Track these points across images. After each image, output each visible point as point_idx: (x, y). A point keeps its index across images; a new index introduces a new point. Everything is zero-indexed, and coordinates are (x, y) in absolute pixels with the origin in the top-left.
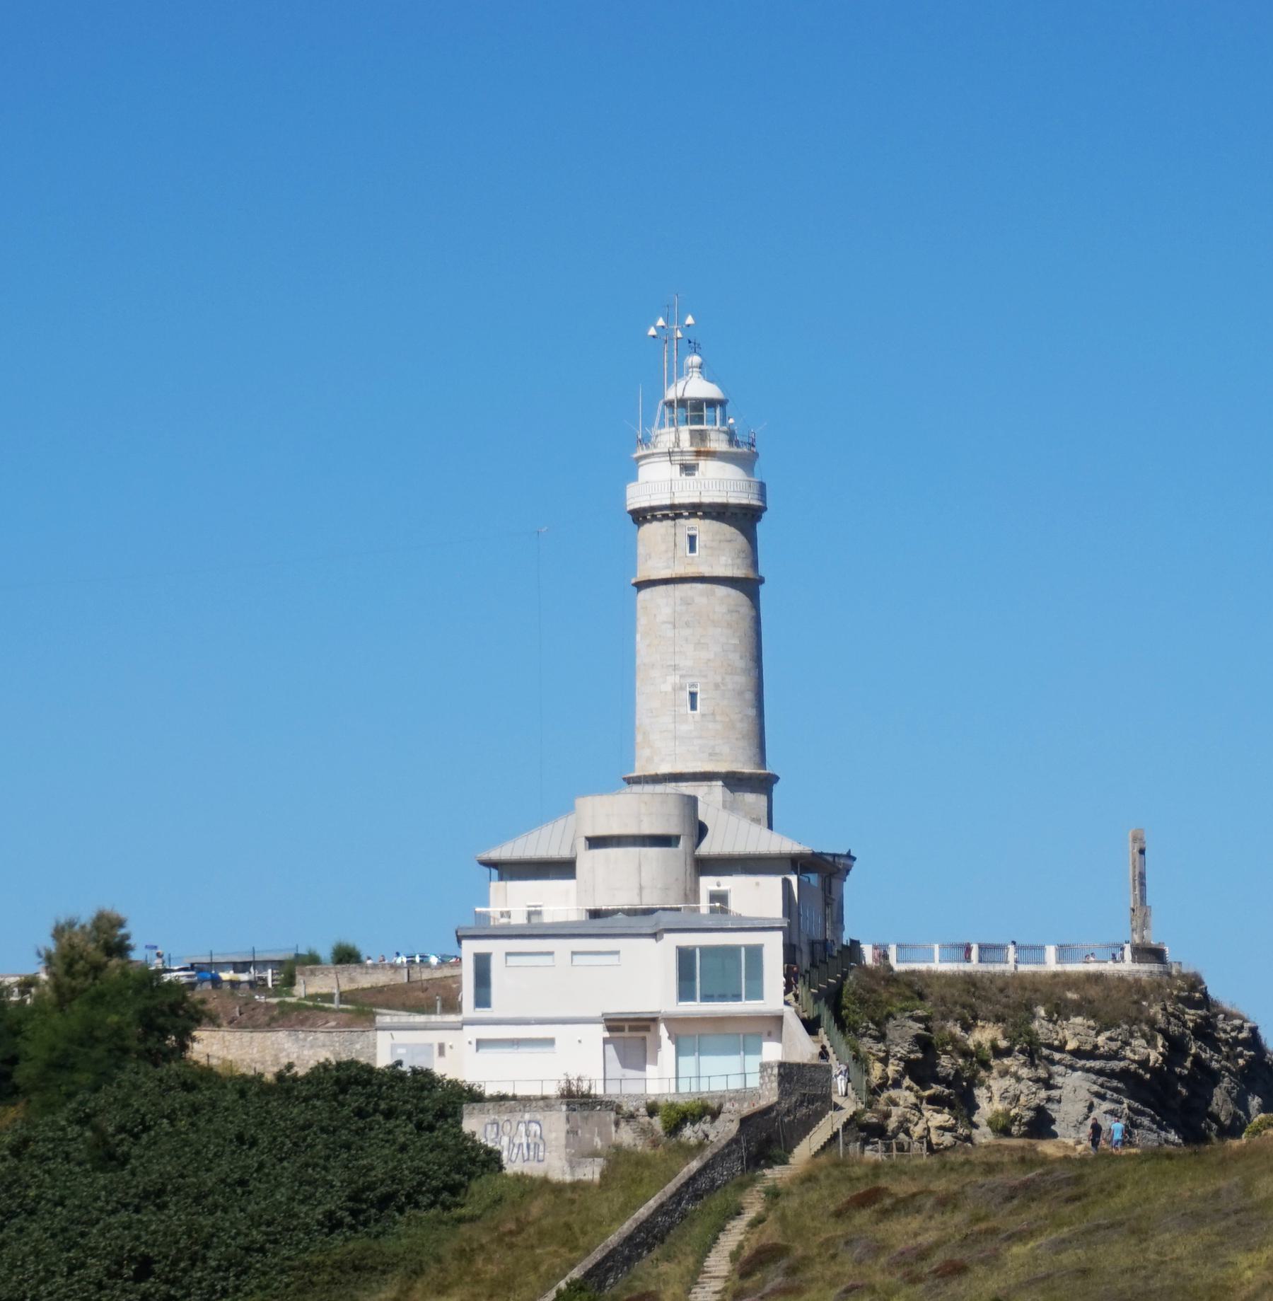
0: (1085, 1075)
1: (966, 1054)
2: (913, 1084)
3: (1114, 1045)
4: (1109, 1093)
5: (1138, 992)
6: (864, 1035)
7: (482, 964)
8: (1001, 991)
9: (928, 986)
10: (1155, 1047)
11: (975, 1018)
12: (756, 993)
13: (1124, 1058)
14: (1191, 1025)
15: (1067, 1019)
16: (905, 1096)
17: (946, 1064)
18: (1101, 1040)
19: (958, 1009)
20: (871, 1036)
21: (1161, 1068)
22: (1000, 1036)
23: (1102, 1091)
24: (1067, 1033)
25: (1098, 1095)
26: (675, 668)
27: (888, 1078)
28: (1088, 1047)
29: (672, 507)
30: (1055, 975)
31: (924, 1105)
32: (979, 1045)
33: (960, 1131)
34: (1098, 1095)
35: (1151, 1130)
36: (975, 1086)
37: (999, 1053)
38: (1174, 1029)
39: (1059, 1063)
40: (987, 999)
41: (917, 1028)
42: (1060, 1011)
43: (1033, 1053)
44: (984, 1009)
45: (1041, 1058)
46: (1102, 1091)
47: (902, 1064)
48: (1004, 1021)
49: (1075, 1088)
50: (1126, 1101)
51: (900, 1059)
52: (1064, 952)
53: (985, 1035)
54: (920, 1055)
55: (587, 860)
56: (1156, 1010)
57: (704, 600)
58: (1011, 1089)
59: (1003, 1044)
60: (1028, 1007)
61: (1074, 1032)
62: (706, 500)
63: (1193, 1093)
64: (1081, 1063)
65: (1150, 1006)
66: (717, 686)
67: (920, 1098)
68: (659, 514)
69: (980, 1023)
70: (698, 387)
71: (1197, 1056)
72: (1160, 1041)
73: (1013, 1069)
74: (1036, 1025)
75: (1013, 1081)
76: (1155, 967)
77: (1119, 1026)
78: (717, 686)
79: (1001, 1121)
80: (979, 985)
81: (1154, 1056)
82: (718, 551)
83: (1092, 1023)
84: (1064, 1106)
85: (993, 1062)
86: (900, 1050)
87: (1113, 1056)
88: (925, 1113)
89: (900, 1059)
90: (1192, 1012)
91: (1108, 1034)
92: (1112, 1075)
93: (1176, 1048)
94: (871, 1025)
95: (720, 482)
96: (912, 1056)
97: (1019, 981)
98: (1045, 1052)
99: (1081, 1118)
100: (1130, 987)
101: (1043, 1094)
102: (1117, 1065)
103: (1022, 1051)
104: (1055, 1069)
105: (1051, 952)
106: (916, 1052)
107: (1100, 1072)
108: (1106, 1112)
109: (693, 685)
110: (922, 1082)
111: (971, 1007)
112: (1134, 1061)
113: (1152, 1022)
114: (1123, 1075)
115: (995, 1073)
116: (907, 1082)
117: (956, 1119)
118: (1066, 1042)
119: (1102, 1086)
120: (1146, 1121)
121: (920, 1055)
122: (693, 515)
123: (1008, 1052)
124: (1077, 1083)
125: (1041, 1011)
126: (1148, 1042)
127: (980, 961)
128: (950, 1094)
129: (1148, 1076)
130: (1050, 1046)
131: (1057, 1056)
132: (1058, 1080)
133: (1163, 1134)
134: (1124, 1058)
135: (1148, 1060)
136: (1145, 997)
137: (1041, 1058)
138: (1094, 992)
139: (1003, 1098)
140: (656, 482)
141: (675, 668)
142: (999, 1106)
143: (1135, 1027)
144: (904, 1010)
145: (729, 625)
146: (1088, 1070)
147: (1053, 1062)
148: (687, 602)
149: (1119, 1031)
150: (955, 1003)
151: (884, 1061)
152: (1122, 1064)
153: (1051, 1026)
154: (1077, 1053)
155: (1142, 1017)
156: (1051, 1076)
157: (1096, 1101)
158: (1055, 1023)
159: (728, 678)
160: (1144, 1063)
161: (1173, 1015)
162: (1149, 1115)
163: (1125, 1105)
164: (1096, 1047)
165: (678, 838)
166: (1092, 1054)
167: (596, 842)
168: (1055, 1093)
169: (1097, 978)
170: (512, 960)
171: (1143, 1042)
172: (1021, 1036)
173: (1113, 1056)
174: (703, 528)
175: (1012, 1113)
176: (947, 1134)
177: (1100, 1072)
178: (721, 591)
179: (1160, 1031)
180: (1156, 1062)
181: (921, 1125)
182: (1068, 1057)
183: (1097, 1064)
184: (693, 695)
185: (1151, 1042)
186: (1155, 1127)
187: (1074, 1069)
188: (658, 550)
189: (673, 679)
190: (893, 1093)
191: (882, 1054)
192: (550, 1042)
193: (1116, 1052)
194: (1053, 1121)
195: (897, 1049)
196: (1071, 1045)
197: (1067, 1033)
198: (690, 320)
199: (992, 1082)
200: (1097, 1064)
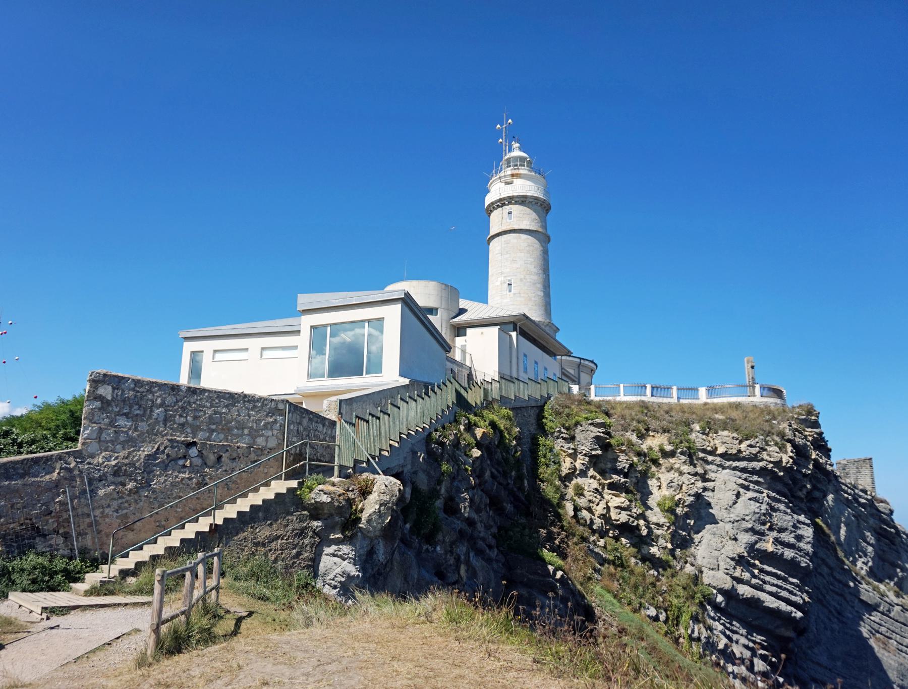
0: (732, 472)
1: (639, 454)
2: (596, 474)
3: (754, 451)
4: (752, 486)
5: (769, 414)
6: (558, 438)
8: (667, 412)
9: (613, 408)
10: (786, 452)
11: (647, 430)
12: (376, 367)
13: (762, 460)
14: (810, 439)
15: (716, 432)
16: (589, 483)
17: (623, 462)
18: (743, 446)
19: (635, 423)
20: (564, 439)
21: (791, 468)
22: (666, 442)
23: (747, 484)
24: (716, 442)
25: (742, 486)
26: (502, 273)
27: (575, 469)
28: (734, 452)
29: (500, 200)
30: (706, 404)
31: (606, 490)
32: (651, 449)
33: (634, 510)
34: (742, 486)
35: (786, 513)
36: (648, 478)
38: (799, 440)
39: (711, 463)
40: (657, 418)
41: (596, 431)
42: (709, 428)
43: (691, 455)
45: (698, 459)
46: (747, 484)
47: (587, 459)
48: (668, 431)
49: (724, 485)
50: (765, 491)
51: (585, 455)
52: (711, 391)
53: (655, 442)
54: (599, 452)
56: (784, 426)
57: (515, 241)
58: (675, 480)
59: (669, 448)
60: (688, 424)
61: (723, 441)
62: (515, 194)
63: (814, 487)
64: (728, 463)
65: (779, 423)
66: (521, 280)
67: (603, 486)
68: (495, 206)
69: (651, 433)
71: (815, 460)
72: (789, 447)
73: (676, 466)
74: (693, 436)
75: (677, 475)
76: (779, 401)
77: (756, 437)
78: (521, 280)
79: (668, 504)
80: (651, 408)
82: (524, 218)
83: (735, 435)
84: (717, 494)
85: (661, 461)
86: (585, 448)
87: (754, 458)
88: (606, 496)
89: (585, 455)
90: (810, 430)
91: (748, 442)
92: (753, 472)
93: (800, 453)
94: (563, 430)
96: (594, 453)
97: (682, 409)
98: (701, 455)
99: (731, 503)
100: (762, 411)
101: (700, 484)
102: (757, 465)
103: (682, 453)
104: (708, 467)
105: (703, 391)
106: (596, 449)
107: (744, 470)
108: (750, 499)
109: (510, 280)
110: (603, 473)
111: (644, 422)
112: (770, 462)
113: (782, 435)
114: (762, 472)
115: (663, 469)
116: (591, 472)
117: (630, 501)
118: (716, 448)
119: (745, 480)
120: (782, 507)
121: (599, 452)
122: (510, 203)
123: (672, 454)
124: (727, 478)
125: (697, 427)
126: (780, 448)
127: (652, 396)
128: (626, 482)
129: (782, 474)
130: (704, 451)
131: (710, 458)
132: (711, 475)
133: (795, 516)
134: (762, 460)
135: (781, 461)
136: (774, 418)
137: (698, 459)
138: (735, 414)
139: (669, 486)
141: (502, 273)
142: (666, 492)
143: (768, 438)
144: (587, 419)
145: (528, 252)
146: (735, 469)
147: (707, 462)
148: (507, 243)
149: (757, 440)
150: (633, 419)
151: (574, 456)
152: (761, 464)
153: (704, 437)
154: (724, 456)
155: (773, 431)
156: (706, 472)
157: (742, 491)
158: (707, 435)
159: (527, 277)
160: (778, 464)
161: (797, 430)
162: (784, 502)
163: (765, 495)
164: (739, 451)
165: (437, 309)
166: (737, 457)
168: (709, 485)
169: (737, 406)
170: (219, 356)
171: (777, 449)
172: (681, 442)
173: (754, 458)
174: (515, 209)
175: (677, 498)
176: (623, 512)
177: (744, 470)
178: (523, 236)
179: (789, 441)
180: (787, 463)
181: (602, 505)
182: (719, 459)
183: (742, 464)
184: (510, 284)
185: (782, 448)
186: (789, 511)
187: (724, 468)
189: (501, 279)
190: (580, 481)
191: (571, 451)
193: (756, 455)
194: (709, 505)
195: (583, 448)
196: (721, 450)
197: (716, 442)
198: (510, 121)
199: (660, 476)
200: (742, 464)
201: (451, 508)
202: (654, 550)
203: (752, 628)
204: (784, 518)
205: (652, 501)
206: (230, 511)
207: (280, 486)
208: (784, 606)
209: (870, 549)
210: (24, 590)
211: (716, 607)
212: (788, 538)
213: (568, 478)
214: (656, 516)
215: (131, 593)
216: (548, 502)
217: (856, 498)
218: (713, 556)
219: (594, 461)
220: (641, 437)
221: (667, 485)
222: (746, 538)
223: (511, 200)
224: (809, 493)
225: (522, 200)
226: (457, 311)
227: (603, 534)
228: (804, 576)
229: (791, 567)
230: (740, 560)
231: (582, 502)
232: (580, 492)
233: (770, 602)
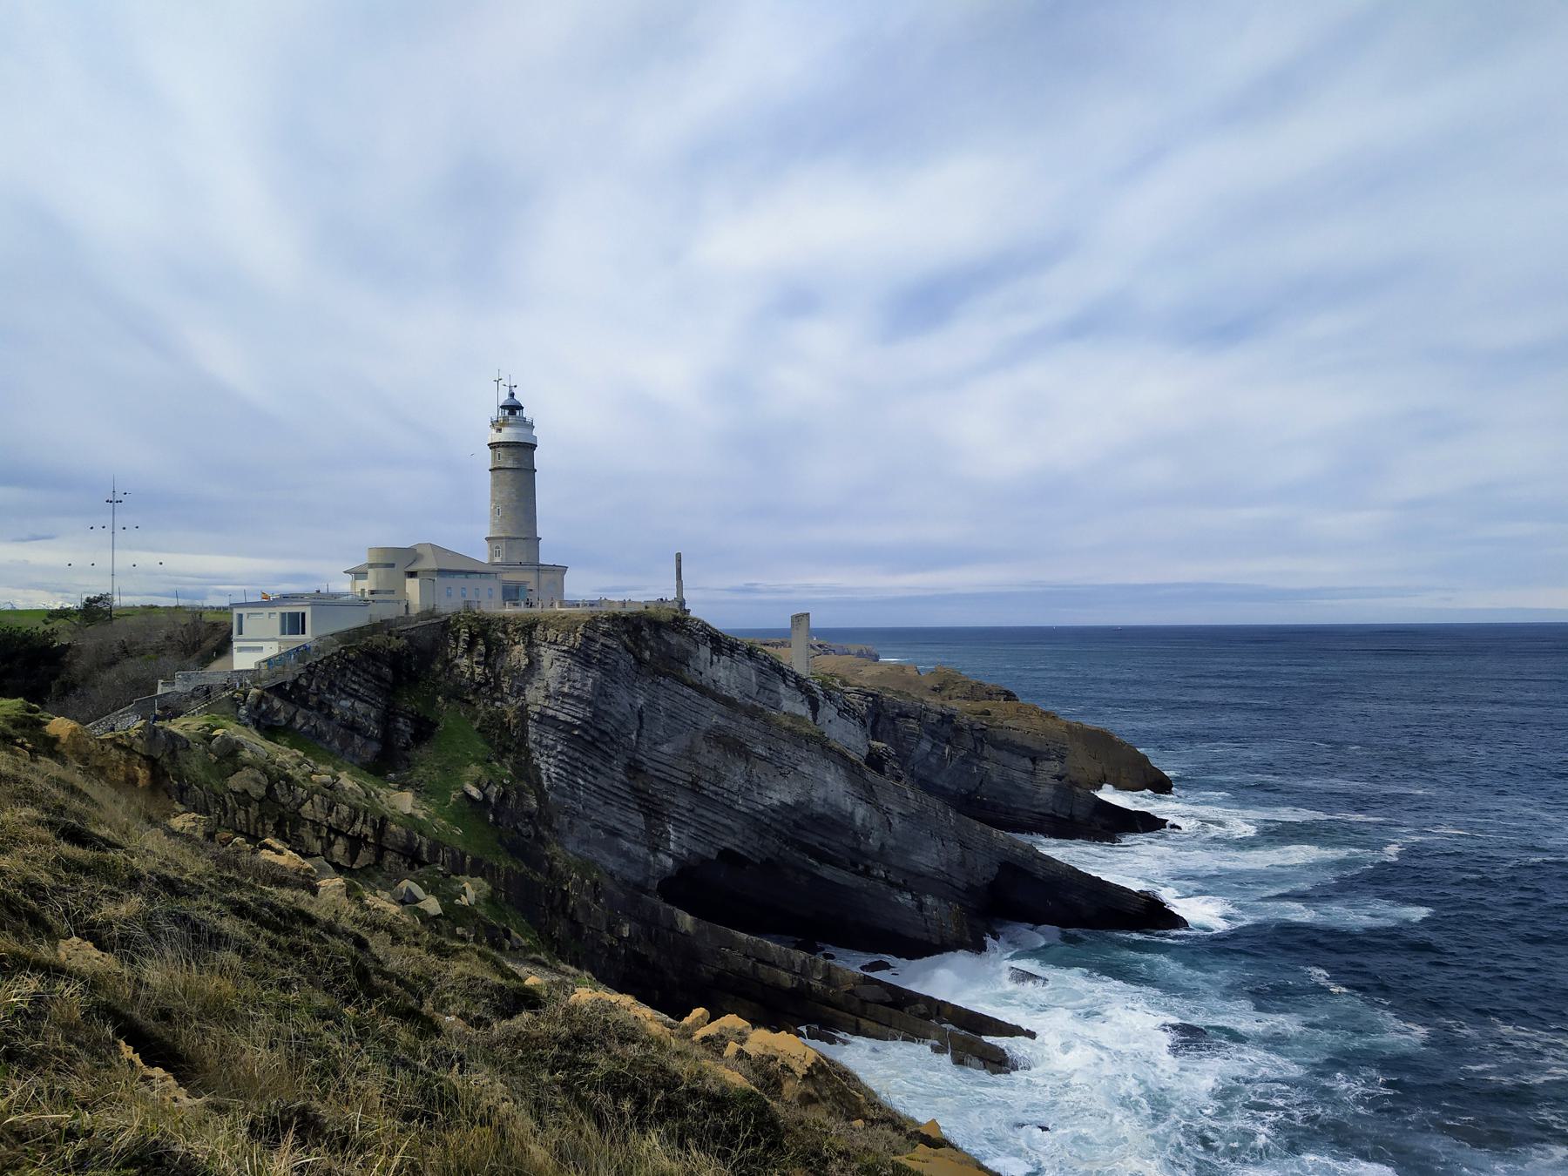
208: (569, 719)
212: (578, 685)
229: (579, 699)
233: (562, 717)
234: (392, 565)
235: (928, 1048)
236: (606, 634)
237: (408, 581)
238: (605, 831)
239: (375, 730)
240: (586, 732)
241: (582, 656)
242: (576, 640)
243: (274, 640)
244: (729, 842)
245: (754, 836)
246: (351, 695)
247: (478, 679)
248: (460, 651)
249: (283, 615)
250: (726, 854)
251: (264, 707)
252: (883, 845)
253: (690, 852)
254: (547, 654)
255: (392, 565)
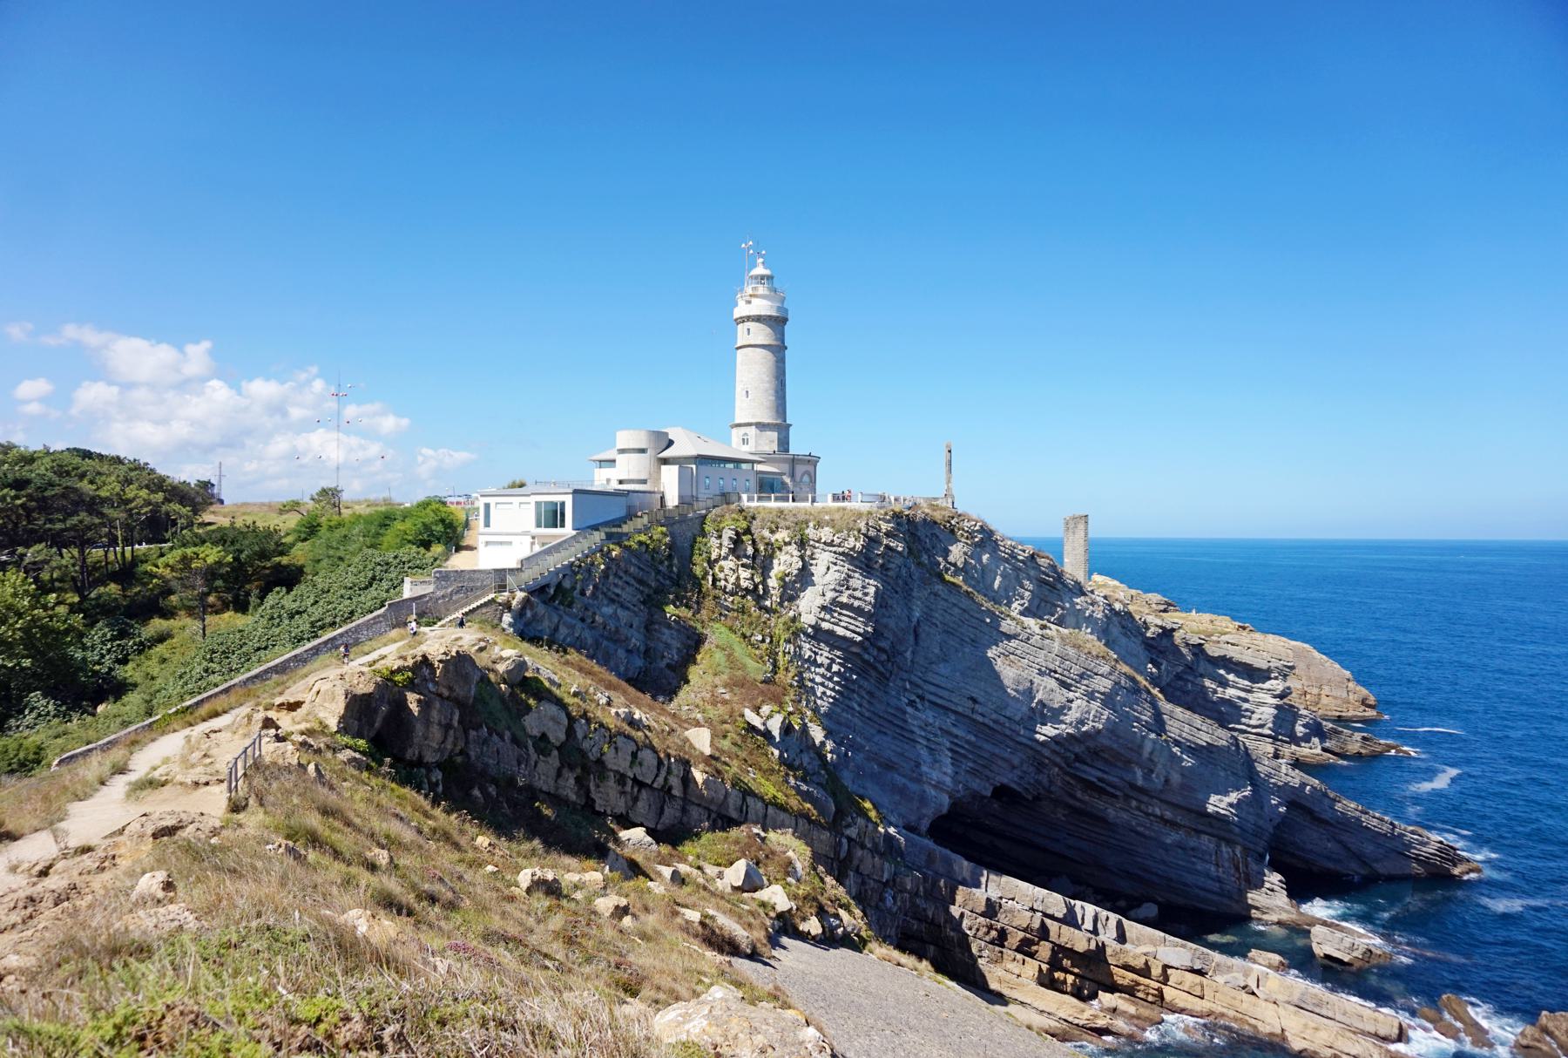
7: (487, 506)
16: (728, 564)
37: (787, 544)
42: (819, 525)
44: (782, 523)
53: (783, 535)
55: (620, 458)
60: (807, 523)
61: (826, 534)
70: (760, 270)
81: (859, 546)
82: (761, 334)
95: (762, 307)
110: (738, 558)
114: (843, 554)
140: (741, 310)
142: (782, 568)
167: (622, 451)
174: (751, 325)
188: (743, 334)
192: (510, 543)
201: (583, 593)
202: (768, 603)
203: (832, 647)
204: (856, 582)
205: (772, 574)
206: (474, 605)
207: (492, 596)
208: (849, 634)
209: (1027, 594)
210: (118, 461)
211: (806, 634)
212: (858, 594)
213: (716, 561)
214: (773, 582)
215: (345, 621)
216: (695, 577)
217: (1013, 556)
218: (808, 606)
219: (733, 551)
220: (772, 532)
221: (785, 563)
222: (830, 595)
223: (749, 318)
224: (882, 566)
225: (758, 319)
226: (664, 444)
227: (732, 594)
228: (870, 617)
229: (859, 611)
230: (823, 608)
231: (721, 576)
232: (722, 570)
233: (840, 631)
234: (643, 451)
235: (230, 494)
236: (888, 534)
237: (664, 468)
238: (880, 765)
239: (636, 640)
240: (865, 649)
241: (863, 561)
242: (855, 543)
243: (525, 533)
244: (1007, 778)
245: (1031, 769)
246: (612, 601)
247: (744, 584)
248: (724, 551)
249: (538, 504)
250: (1001, 792)
251: (529, 614)
252: (1167, 781)
253: (966, 788)
254: (823, 558)
255: (643, 451)
